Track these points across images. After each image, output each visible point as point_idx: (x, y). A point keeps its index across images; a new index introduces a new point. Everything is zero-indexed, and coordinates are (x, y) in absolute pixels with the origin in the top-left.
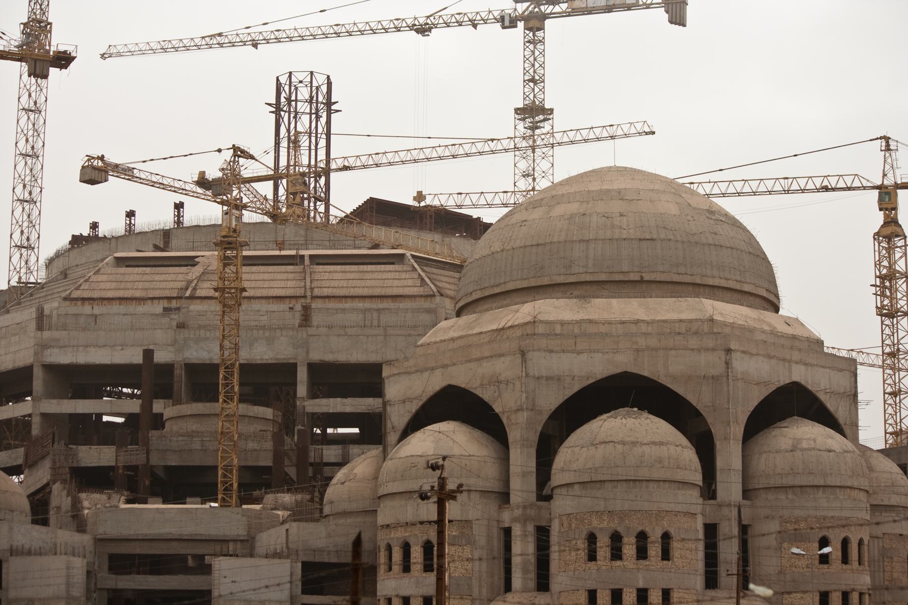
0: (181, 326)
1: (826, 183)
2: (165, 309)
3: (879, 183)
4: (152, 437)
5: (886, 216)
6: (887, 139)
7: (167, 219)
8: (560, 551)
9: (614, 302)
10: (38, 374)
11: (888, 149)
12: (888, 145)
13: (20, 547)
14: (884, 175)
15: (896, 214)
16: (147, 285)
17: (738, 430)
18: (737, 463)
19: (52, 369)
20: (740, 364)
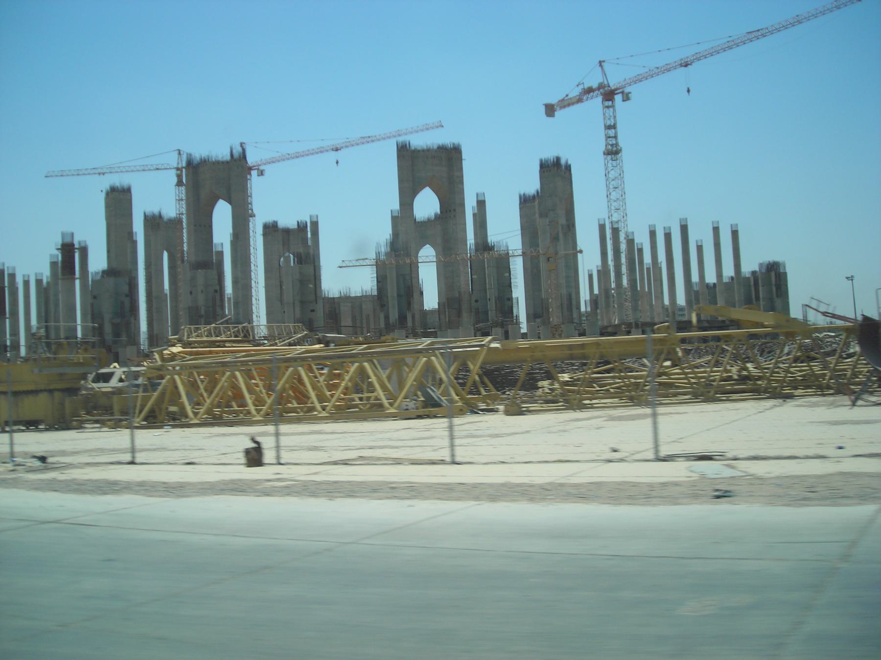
1: (158, 167)
3: (176, 166)
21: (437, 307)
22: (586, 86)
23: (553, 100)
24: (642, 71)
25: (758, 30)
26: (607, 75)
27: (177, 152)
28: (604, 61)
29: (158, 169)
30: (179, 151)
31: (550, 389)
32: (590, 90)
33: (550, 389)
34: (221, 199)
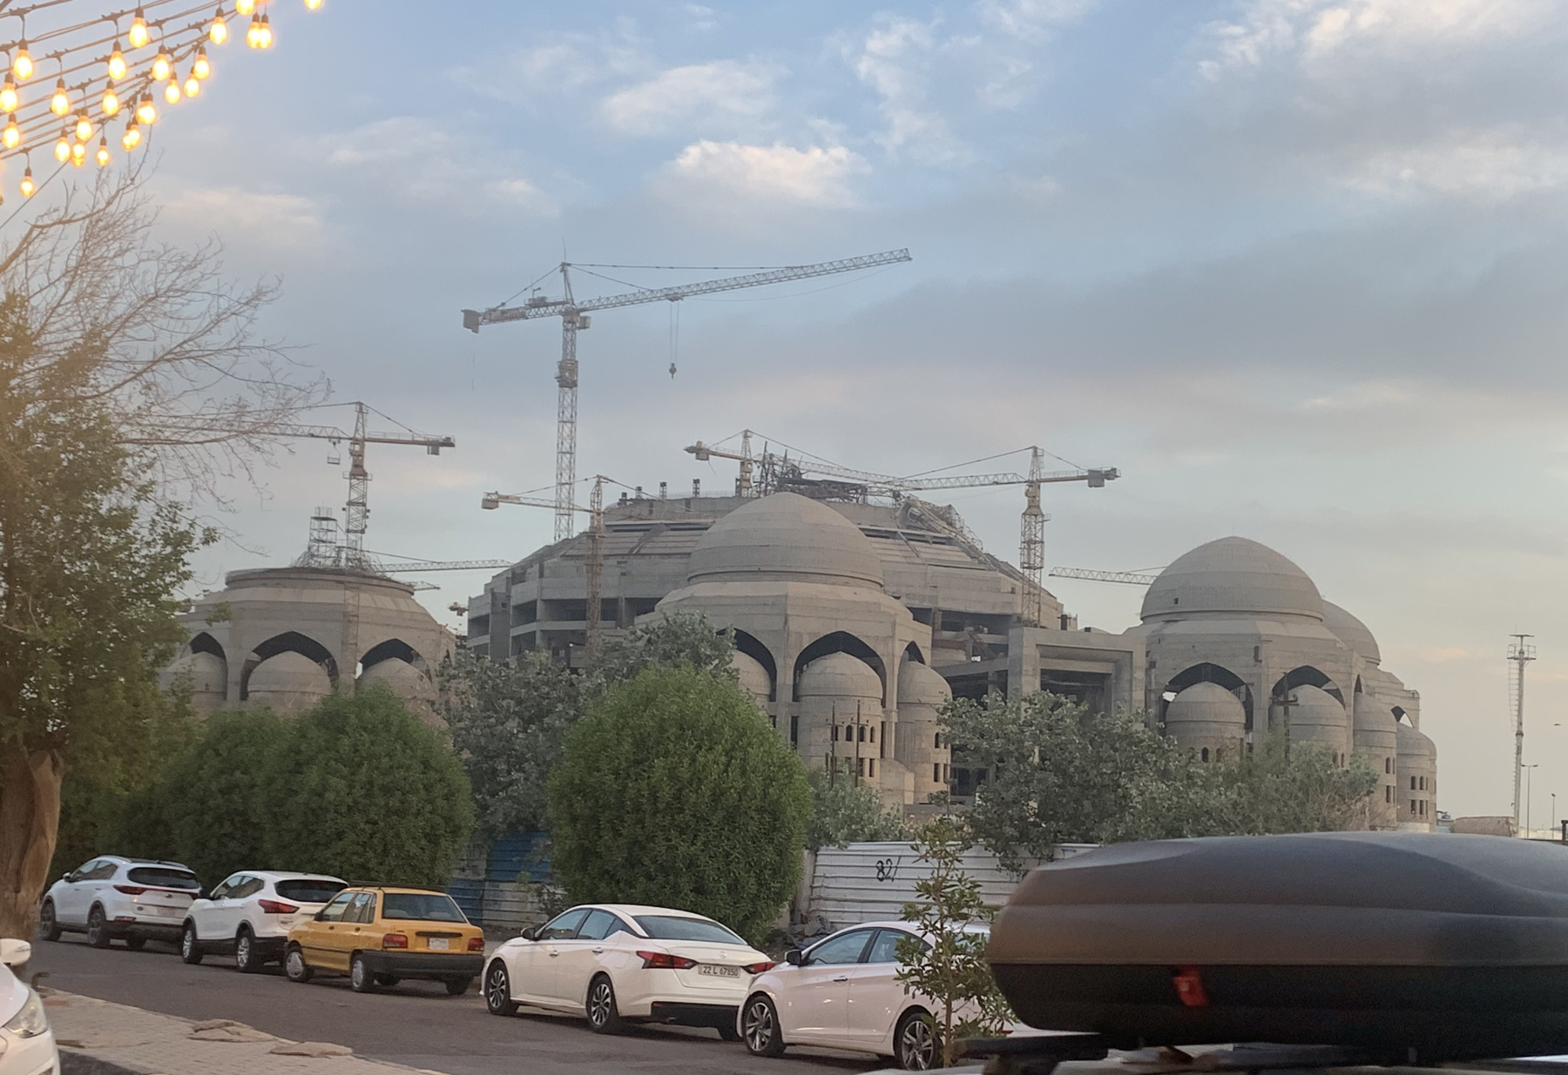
0: (623, 574)
1: (312, 432)
2: (619, 563)
3: (352, 436)
4: (104, 579)
5: (354, 461)
6: (360, 404)
7: (688, 491)
8: (1131, 780)
9: (791, 583)
10: (539, 605)
11: (361, 411)
12: (361, 409)
13: (166, 662)
14: (357, 430)
15: (362, 460)
16: (614, 546)
17: (792, 662)
18: (790, 681)
19: (549, 602)
20: (794, 625)
21: (86, 922)
22: (538, 294)
23: (481, 308)
24: (629, 291)
25: (802, 267)
26: (572, 288)
27: (1031, 451)
28: (569, 265)
29: (312, 436)
30: (1035, 449)
31: (150, 389)
32: (539, 303)
33: (150, 389)
34: (168, 103)
